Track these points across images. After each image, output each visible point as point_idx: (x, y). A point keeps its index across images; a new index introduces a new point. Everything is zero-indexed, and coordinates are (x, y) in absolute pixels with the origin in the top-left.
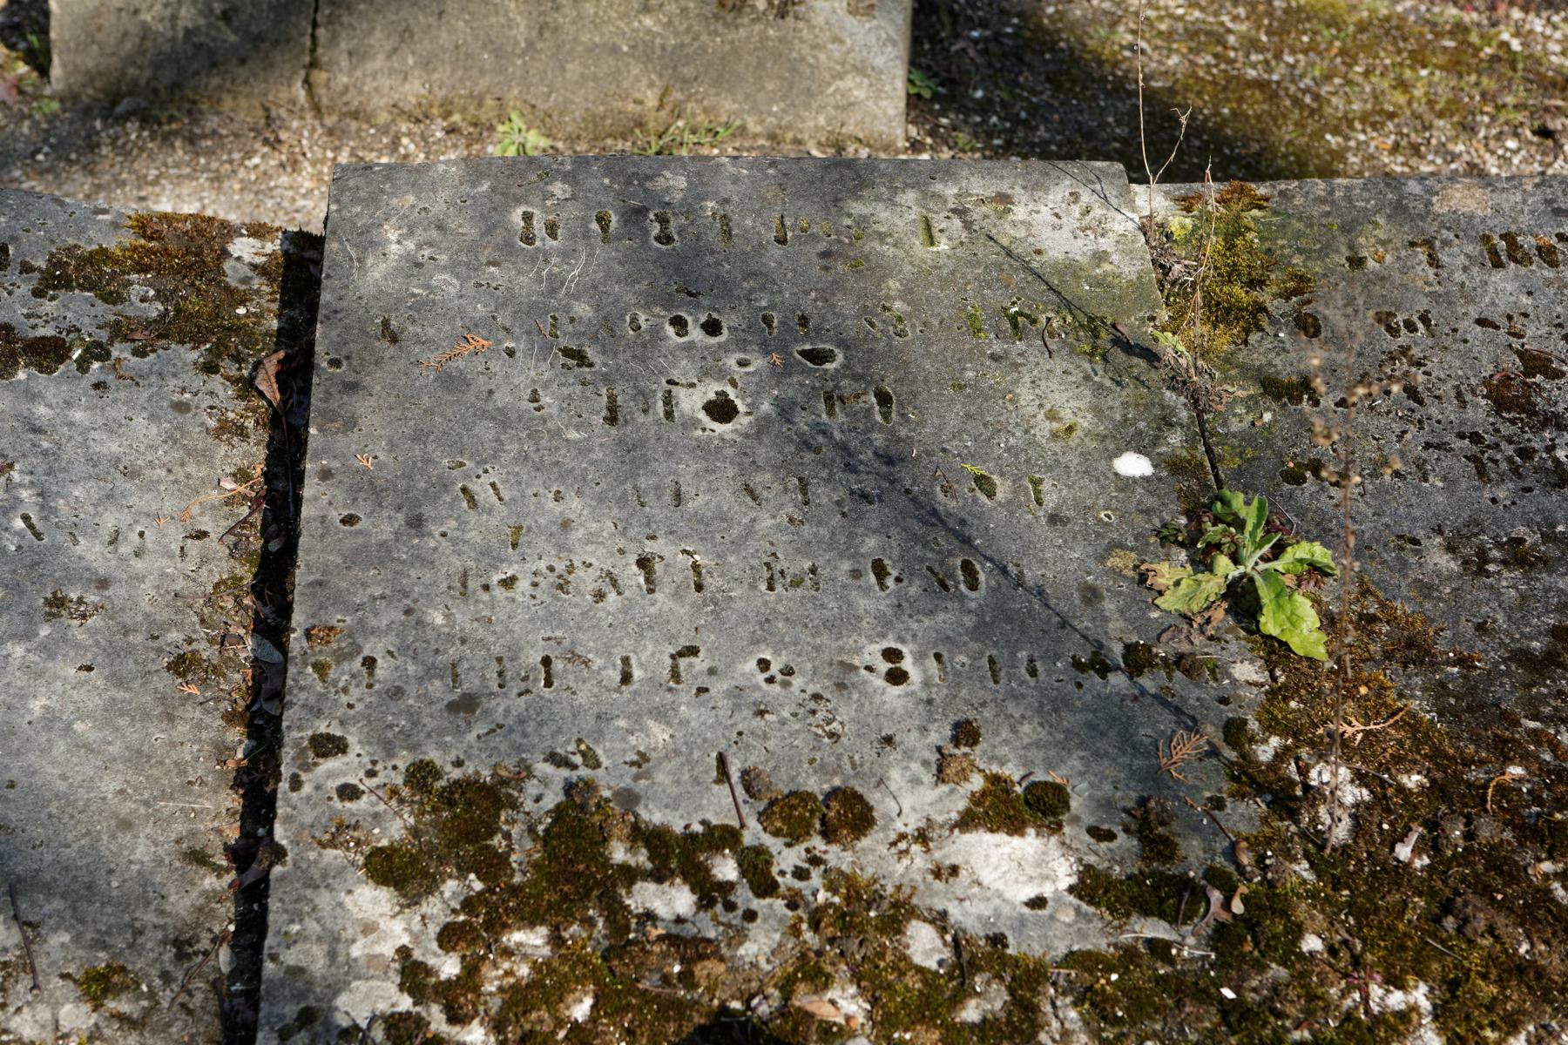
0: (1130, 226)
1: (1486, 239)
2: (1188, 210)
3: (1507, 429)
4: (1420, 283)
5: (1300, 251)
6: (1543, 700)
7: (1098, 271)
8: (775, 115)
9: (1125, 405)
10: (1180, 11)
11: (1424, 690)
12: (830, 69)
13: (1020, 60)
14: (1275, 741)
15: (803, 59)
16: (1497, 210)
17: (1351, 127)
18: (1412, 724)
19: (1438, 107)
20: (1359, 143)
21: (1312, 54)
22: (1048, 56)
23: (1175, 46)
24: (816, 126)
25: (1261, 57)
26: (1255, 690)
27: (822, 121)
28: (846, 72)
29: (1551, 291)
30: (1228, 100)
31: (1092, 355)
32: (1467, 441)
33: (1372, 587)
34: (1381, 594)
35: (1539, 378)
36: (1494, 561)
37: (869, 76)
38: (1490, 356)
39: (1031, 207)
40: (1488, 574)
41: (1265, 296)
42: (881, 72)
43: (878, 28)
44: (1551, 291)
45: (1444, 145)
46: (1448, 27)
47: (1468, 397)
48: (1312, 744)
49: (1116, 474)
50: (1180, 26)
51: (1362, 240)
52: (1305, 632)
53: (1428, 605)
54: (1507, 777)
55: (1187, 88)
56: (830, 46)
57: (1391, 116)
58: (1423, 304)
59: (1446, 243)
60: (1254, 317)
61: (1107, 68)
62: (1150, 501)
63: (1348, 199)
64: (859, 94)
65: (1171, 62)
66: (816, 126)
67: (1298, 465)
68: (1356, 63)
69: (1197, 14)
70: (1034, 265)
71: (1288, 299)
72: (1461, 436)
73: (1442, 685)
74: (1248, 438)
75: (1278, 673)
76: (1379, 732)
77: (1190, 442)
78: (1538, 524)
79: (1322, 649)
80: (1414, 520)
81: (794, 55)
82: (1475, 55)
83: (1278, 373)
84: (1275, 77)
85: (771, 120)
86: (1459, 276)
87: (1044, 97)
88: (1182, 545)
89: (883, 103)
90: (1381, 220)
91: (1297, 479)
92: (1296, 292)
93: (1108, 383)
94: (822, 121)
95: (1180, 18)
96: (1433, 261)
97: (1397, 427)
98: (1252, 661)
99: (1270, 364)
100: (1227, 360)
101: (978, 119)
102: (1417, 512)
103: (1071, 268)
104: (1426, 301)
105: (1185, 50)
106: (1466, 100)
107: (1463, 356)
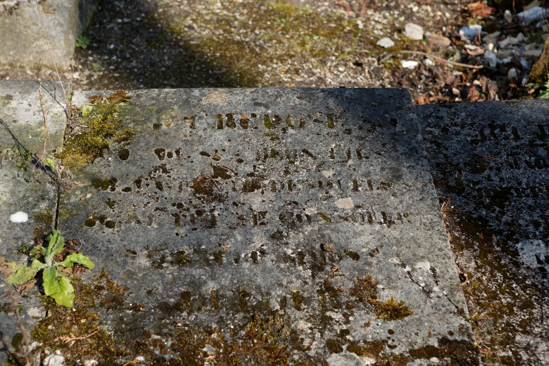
0: (62, 109)
1: (219, 116)
2: (93, 102)
3: (195, 202)
4: (182, 136)
5: (134, 121)
6: (165, 325)
7: (39, 130)
8: (12, 56)
9: (27, 190)
10: (218, 11)
11: (113, 321)
12: (33, 36)
13: (138, 32)
14: (35, 344)
15: (21, 32)
16: (229, 103)
17: (271, 61)
18: (100, 337)
19: (314, 53)
20: (273, 68)
21: (268, 30)
22: (151, 30)
23: (209, 26)
24: (29, 61)
25: (245, 31)
26: (35, 320)
27: (31, 58)
28: (40, 38)
29: (239, 140)
30: (221, 49)
31: (20, 168)
32: (175, 207)
33: (106, 273)
34: (109, 277)
35: (219, 178)
36: (167, 262)
37: (49, 40)
38: (201, 167)
39: (20, 101)
40: (162, 268)
41: (110, 142)
42: (54, 38)
43: (54, 19)
44: (239, 140)
45: (310, 69)
46: (335, 18)
47: (184, 187)
48: (51, 345)
49: (10, 221)
50: (215, 18)
51: (164, 116)
52: (66, 294)
53: (129, 282)
54: (134, 362)
55: (205, 44)
56: (32, 27)
57: (291, 56)
58: (180, 145)
59: (201, 118)
60: (99, 151)
61: (175, 35)
62: (21, 234)
63: (165, 98)
64: (46, 47)
65: (204, 33)
66: (29, 61)
67: (94, 218)
68: (287, 34)
69: (225, 12)
70: (11, 127)
71: (120, 142)
72: (174, 205)
73: (121, 318)
74: (76, 206)
75: (49, 312)
76: (83, 340)
77: (50, 207)
78: (194, 245)
79: (71, 302)
80: (138, 243)
81: (17, 30)
82: (342, 30)
83: (101, 176)
84: (247, 40)
85: (10, 58)
86: (201, 133)
87: (142, 48)
88: (25, 253)
89: (57, 51)
90: (176, 107)
91: (91, 224)
92: (125, 139)
93: (23, 180)
94: (31, 58)
95: (217, 14)
96: (192, 126)
97: (146, 201)
98: (39, 307)
99: (100, 172)
100: (81, 170)
101: (106, 57)
102: (140, 239)
103: (27, 129)
104: (181, 144)
105: (212, 28)
106: (329, 49)
107: (188, 169)
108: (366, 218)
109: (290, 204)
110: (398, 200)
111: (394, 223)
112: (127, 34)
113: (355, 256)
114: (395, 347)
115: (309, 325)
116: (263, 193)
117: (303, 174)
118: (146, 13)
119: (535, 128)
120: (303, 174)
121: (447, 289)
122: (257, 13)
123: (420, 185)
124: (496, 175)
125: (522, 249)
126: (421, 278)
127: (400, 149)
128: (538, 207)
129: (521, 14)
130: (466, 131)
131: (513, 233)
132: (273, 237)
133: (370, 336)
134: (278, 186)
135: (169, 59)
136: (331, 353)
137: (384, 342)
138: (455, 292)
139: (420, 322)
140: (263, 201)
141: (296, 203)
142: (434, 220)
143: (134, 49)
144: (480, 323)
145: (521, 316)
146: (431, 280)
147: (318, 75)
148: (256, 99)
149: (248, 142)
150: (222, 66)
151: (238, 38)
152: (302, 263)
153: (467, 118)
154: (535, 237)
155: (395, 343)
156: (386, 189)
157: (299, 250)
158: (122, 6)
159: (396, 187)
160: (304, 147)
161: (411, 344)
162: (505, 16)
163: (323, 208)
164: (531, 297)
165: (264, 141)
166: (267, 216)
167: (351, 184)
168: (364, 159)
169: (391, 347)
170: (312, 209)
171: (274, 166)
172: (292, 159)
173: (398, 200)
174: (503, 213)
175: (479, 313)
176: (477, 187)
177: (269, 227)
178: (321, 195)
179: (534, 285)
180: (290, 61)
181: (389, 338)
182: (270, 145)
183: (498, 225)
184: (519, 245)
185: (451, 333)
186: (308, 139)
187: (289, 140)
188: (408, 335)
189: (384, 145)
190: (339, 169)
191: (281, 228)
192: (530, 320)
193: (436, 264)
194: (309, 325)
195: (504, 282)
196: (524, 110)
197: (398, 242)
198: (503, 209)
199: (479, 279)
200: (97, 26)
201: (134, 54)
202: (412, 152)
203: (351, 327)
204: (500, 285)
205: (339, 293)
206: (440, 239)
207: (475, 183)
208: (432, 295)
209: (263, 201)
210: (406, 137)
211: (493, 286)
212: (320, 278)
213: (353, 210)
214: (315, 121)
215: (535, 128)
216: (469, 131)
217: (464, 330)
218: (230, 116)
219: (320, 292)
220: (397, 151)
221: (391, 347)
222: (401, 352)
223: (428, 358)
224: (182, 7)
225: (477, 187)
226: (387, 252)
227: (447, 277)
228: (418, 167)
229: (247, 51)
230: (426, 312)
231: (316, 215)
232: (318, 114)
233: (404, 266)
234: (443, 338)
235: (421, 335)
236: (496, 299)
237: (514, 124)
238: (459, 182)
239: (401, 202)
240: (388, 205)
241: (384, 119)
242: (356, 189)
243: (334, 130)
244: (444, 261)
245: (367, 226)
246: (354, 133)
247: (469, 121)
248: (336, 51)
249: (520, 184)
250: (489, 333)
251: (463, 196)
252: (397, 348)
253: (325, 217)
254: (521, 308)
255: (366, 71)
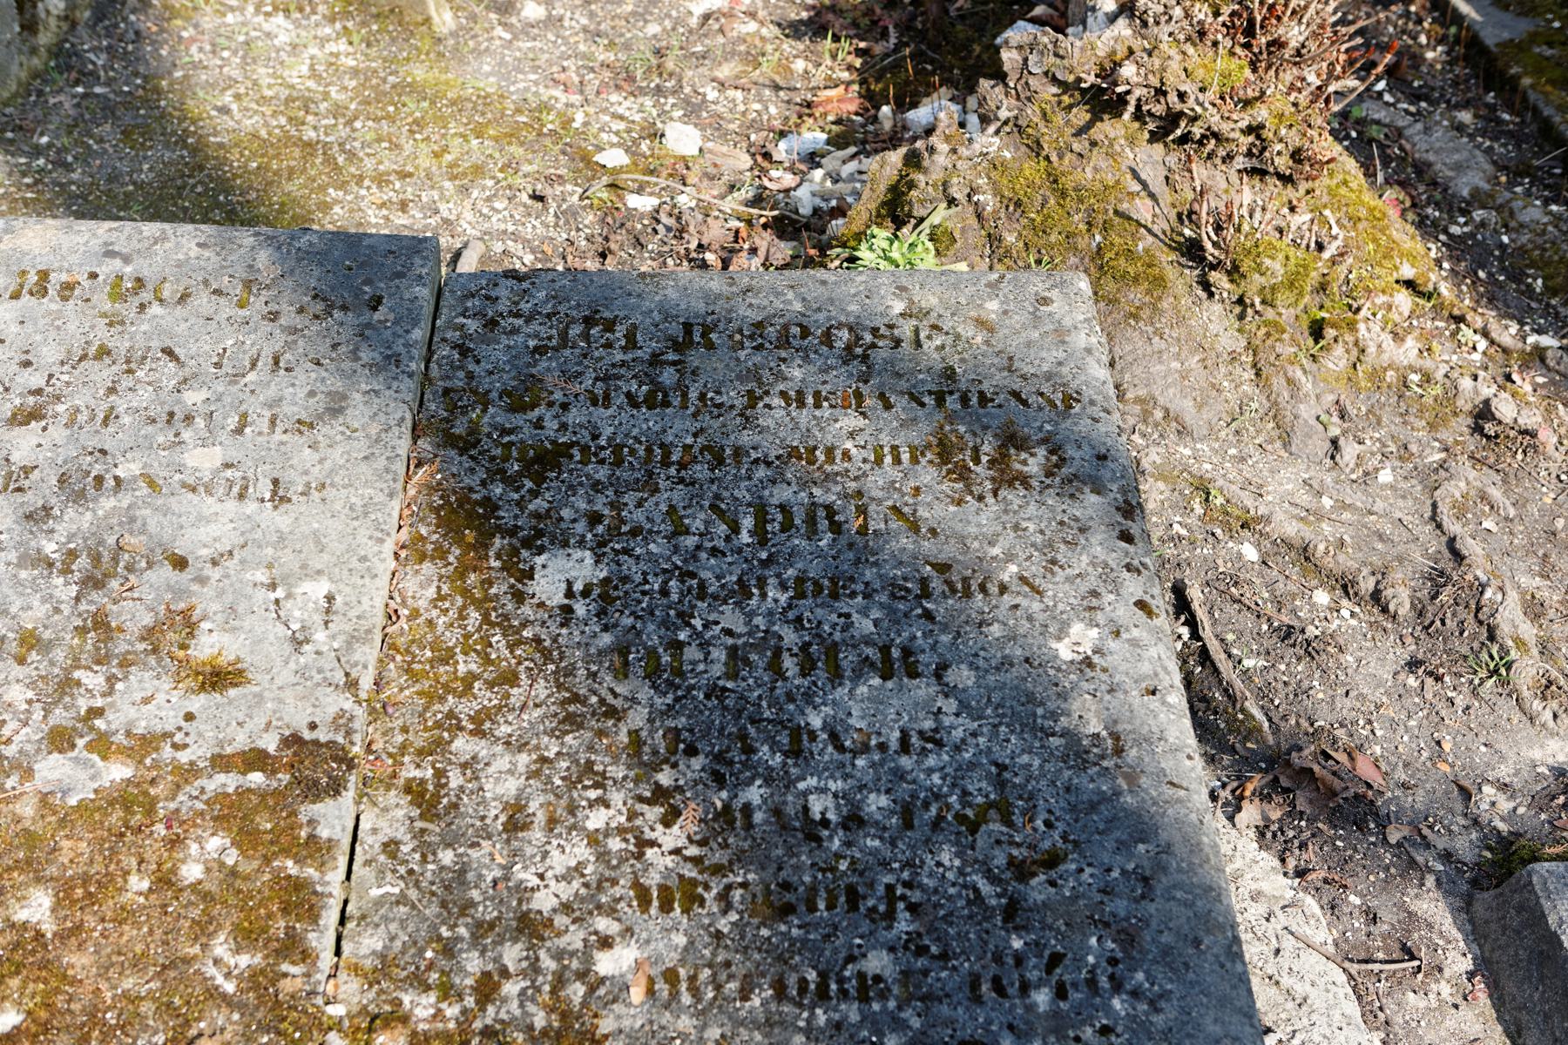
13: (113, 113)
17: (359, 182)
29: (42, 322)
69: (311, 84)
95: (292, 87)
101: (23, 160)
108: (236, 490)
109: (91, 453)
110: (317, 456)
111: (289, 500)
112: (87, 117)
113: (180, 563)
114: (186, 746)
115: (30, 694)
116: (45, 429)
117: (145, 395)
118: (145, 78)
119: (675, 329)
120: (145, 395)
121: (343, 637)
122: (375, 88)
123: (374, 430)
124: (556, 416)
125: (544, 566)
126: (297, 614)
127: (366, 355)
128: (612, 484)
129: (911, 115)
130: (534, 326)
131: (540, 534)
132: (29, 517)
133: (143, 724)
134: (82, 418)
135: (151, 169)
136: (50, 753)
137: (167, 735)
138: (356, 646)
139: (260, 697)
140: (40, 445)
141: (103, 452)
142: (376, 500)
143: (89, 147)
144: (390, 710)
145: (485, 697)
146: (318, 618)
147: (445, 214)
148: (112, 244)
149: (58, 328)
150: (251, 187)
151: (313, 134)
152: (66, 571)
153: (546, 302)
154: (581, 543)
155: (188, 740)
156: (301, 433)
157: (72, 546)
158: (100, 63)
159: (329, 430)
160: (168, 343)
161: (221, 744)
162: (880, 114)
163: (156, 464)
164: (519, 663)
165: (93, 327)
166: (35, 475)
167: (233, 422)
168: (282, 372)
169: (175, 746)
170: (132, 466)
171: (92, 377)
172: (133, 366)
173: (317, 456)
174: (535, 494)
175: (401, 690)
176: (506, 439)
177: (29, 497)
178: (161, 439)
179: (537, 640)
180: (398, 185)
181: (179, 729)
182: (102, 334)
183: (516, 517)
184: (539, 560)
185: (313, 726)
186: (184, 326)
187: (144, 328)
188: (222, 725)
189: (334, 346)
190: (221, 389)
191: (53, 501)
192: (499, 708)
193: (341, 586)
194: (30, 694)
195: (479, 630)
196: (669, 292)
197: (282, 539)
198: (539, 486)
199: (430, 623)
200: (33, 98)
201: (85, 157)
202: (391, 361)
203: (112, 705)
204: (467, 636)
205: (115, 635)
206: (370, 538)
207: (505, 432)
208: (306, 648)
209: (40, 445)
210: (389, 332)
211: (452, 638)
212: (91, 602)
213: (216, 472)
214: (215, 292)
215: (675, 329)
216: (538, 328)
217: (341, 721)
218: (44, 275)
219: (81, 631)
220: (358, 359)
221: (175, 746)
222: (194, 758)
223: (244, 774)
224: (225, 70)
225: (506, 439)
226: (249, 558)
227: (352, 614)
228: (387, 393)
229: (318, 161)
230: (279, 682)
231: (134, 479)
232: (226, 279)
233: (273, 586)
234: (292, 735)
235: (249, 726)
236: (448, 664)
237: (637, 318)
238: (474, 429)
239: (321, 461)
240: (291, 466)
241: (358, 293)
242: (239, 431)
243: (245, 312)
244: (360, 582)
245: (231, 505)
246: (282, 321)
247: (548, 309)
248: (501, 170)
249: (595, 437)
250: (405, 730)
251: (471, 457)
252: (188, 750)
253: (152, 484)
254: (491, 685)
255: (551, 211)
